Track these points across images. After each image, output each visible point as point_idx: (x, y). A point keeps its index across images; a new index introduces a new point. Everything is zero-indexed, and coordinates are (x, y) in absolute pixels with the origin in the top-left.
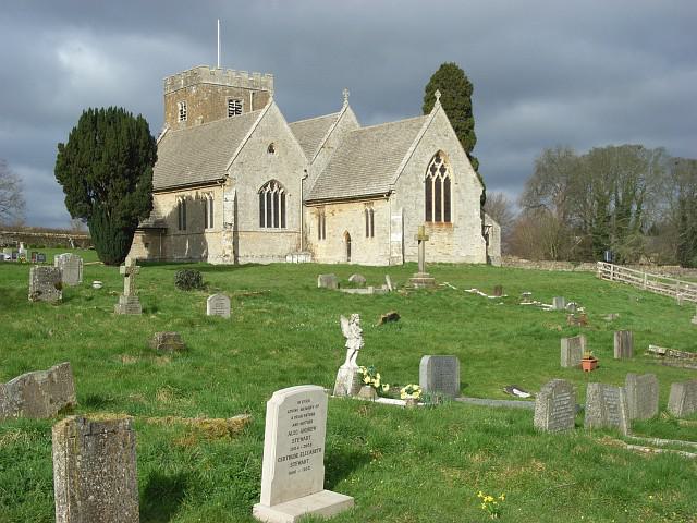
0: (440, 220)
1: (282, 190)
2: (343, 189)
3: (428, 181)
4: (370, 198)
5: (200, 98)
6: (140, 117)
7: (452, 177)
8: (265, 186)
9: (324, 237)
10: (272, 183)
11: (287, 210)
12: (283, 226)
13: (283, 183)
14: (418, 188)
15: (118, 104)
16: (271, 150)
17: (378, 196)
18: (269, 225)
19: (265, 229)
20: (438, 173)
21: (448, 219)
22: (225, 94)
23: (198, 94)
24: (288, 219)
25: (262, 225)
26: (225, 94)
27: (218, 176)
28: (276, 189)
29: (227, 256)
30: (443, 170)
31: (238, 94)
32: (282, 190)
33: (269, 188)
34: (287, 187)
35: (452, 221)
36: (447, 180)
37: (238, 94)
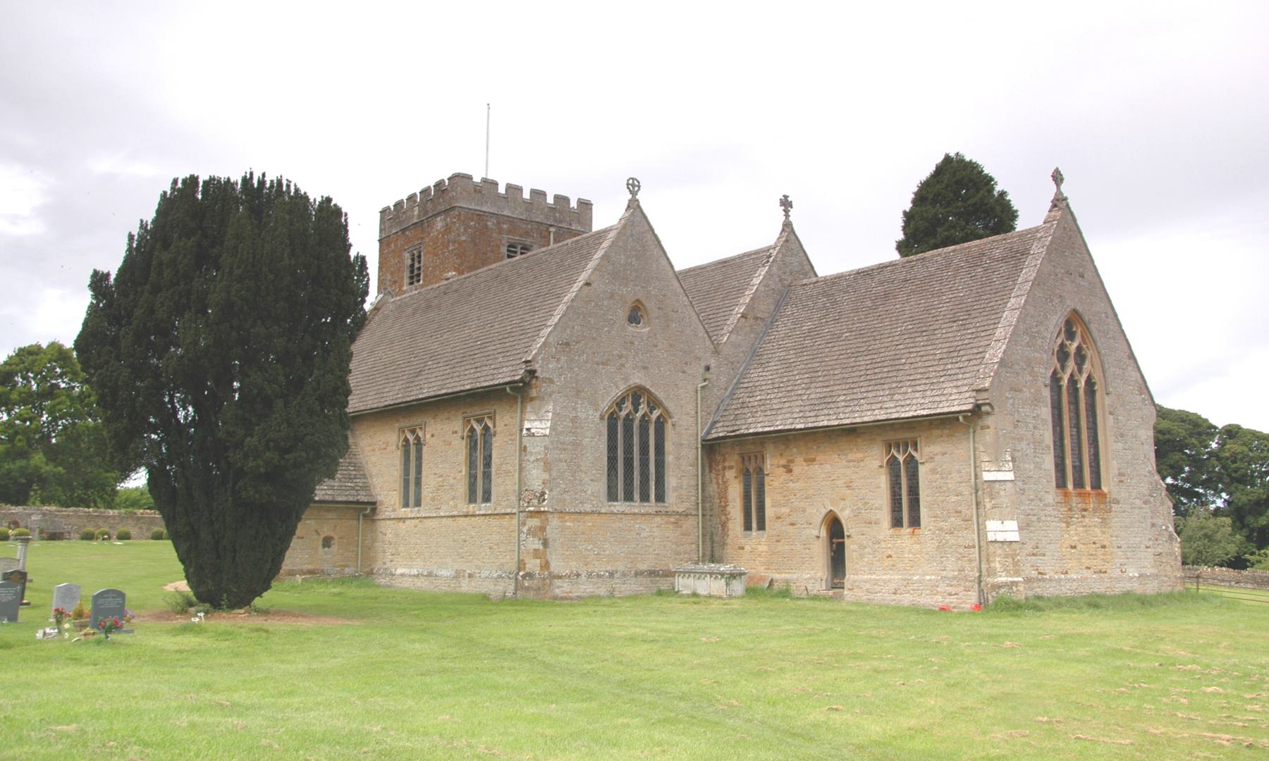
0: (648, 497)
1: (656, 414)
2: (826, 402)
3: (1055, 379)
4: (900, 437)
5: (452, 236)
6: (1003, 194)
7: (1097, 377)
8: (620, 403)
9: (761, 527)
10: (637, 394)
11: (669, 459)
12: (660, 498)
13: (660, 394)
14: (1036, 401)
15: (979, 162)
16: (635, 316)
17: (945, 423)
18: (629, 497)
19: (620, 506)
20: (1071, 365)
21: (1097, 485)
22: (501, 231)
23: (448, 230)
24: (671, 481)
25: (612, 496)
26: (501, 231)
27: (508, 373)
28: (643, 408)
29: (529, 575)
30: (1081, 357)
31: (527, 234)
32: (656, 414)
33: (628, 407)
34: (670, 405)
35: (1105, 489)
36: (1090, 383)
37: (527, 234)
